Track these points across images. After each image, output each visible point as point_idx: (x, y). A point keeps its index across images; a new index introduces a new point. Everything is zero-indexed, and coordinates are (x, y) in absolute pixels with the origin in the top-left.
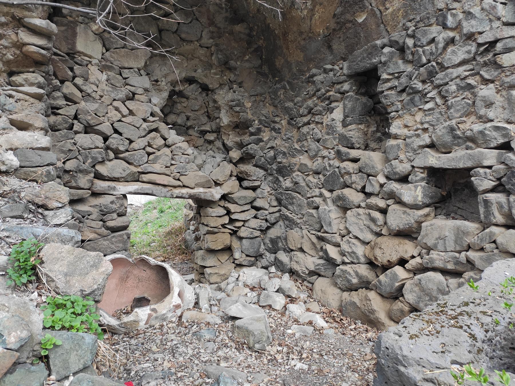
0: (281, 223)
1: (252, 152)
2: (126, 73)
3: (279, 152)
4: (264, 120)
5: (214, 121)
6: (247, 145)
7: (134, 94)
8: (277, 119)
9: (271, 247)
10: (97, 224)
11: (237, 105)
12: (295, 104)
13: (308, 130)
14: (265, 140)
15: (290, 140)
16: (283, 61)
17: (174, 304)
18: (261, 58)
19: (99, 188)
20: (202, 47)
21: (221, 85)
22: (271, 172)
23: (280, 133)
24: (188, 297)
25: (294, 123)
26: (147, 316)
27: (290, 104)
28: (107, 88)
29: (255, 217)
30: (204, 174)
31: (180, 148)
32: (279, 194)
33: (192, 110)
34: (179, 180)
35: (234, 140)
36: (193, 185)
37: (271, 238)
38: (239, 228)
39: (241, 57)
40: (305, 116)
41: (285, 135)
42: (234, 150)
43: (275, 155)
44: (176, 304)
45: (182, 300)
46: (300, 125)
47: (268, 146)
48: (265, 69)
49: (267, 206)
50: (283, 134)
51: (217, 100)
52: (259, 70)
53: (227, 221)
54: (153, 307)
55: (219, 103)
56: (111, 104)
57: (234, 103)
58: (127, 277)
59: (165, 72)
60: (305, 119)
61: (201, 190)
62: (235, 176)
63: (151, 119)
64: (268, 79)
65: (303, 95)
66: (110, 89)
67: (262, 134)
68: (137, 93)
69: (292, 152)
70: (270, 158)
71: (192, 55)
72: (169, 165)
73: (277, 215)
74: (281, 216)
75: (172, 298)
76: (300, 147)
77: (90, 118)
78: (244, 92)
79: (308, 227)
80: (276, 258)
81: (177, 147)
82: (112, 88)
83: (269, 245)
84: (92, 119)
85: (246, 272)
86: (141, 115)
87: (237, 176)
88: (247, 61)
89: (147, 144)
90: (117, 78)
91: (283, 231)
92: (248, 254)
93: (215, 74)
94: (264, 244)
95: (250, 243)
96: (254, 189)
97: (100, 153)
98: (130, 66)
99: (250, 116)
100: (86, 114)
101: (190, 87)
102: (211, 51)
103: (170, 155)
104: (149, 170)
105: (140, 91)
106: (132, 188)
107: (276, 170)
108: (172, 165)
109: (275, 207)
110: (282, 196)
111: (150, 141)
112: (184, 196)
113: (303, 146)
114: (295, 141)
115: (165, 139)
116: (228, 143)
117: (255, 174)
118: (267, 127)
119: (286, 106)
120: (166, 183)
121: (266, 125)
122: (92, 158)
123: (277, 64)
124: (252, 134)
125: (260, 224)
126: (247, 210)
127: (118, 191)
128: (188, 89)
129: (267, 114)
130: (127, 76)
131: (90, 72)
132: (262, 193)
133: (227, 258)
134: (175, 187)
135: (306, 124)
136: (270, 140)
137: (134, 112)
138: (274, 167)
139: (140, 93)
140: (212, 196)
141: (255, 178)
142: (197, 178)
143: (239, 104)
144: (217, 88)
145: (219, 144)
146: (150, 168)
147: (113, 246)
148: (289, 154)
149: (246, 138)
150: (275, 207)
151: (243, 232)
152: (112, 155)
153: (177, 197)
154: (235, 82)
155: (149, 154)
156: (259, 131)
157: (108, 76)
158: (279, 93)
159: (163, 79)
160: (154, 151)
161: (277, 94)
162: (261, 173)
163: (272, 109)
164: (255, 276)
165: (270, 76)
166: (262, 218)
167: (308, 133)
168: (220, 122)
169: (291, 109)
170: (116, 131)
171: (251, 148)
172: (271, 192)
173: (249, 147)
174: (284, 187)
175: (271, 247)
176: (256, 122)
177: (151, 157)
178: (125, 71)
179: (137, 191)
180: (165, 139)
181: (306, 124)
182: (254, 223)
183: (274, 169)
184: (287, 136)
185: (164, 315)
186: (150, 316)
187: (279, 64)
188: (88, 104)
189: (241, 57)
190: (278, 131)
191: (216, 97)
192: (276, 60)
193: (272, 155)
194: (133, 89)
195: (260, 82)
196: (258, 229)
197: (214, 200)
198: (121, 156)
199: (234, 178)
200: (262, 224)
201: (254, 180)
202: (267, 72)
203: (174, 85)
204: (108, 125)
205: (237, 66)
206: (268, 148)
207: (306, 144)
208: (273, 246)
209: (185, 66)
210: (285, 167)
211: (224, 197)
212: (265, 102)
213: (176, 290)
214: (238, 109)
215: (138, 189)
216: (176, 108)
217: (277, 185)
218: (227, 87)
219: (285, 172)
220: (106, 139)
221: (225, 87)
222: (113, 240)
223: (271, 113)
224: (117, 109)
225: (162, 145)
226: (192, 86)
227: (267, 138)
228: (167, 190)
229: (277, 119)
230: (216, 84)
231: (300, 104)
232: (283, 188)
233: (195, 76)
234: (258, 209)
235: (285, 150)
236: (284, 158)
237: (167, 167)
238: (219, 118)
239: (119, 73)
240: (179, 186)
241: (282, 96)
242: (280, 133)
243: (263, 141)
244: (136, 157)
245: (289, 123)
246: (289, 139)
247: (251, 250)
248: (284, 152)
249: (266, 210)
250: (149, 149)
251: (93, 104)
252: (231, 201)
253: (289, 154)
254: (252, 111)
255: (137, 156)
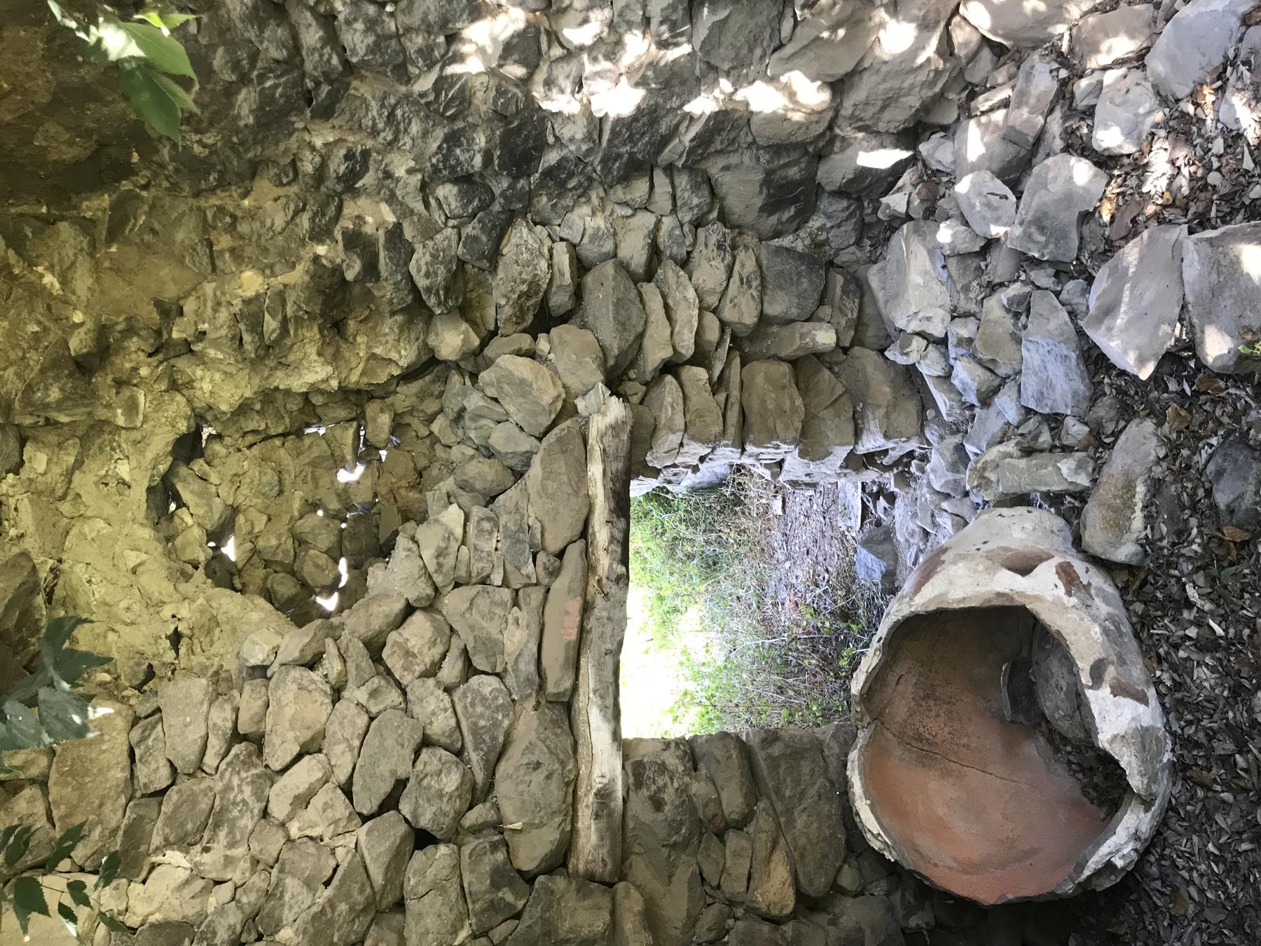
0: (714, 167)
1: (441, 271)
2: (154, 773)
3: (446, 159)
4: (312, 220)
5: (319, 411)
6: (414, 288)
7: (236, 737)
8: (308, 166)
9: (792, 211)
10: (737, 854)
11: (256, 325)
12: (244, 80)
13: (359, 26)
14: (391, 219)
15: (399, 112)
16: (52, 128)
17: (1061, 590)
18: (50, 221)
19: (604, 852)
20: (22, 463)
21: (174, 386)
22: (520, 201)
23: (366, 154)
24: (1023, 536)
25: (325, 89)
26: (1122, 700)
27: (245, 103)
28: (219, 848)
29: (685, 263)
30: (536, 460)
31: (441, 553)
32: (610, 172)
33: (281, 492)
34: (560, 555)
35: (391, 338)
36: (577, 502)
37: (762, 209)
38: (723, 325)
39: (49, 308)
40: (295, 37)
41: (374, 132)
42: (432, 341)
43: (455, 181)
44: (1060, 584)
45: (1041, 560)
46: (335, 60)
47: (419, 206)
48: (97, 205)
49: (647, 220)
50: (369, 144)
51: (236, 400)
52: (102, 232)
53: (702, 373)
54: (1085, 679)
55: (248, 394)
56: (283, 825)
57: (247, 338)
58: (919, 738)
59: (136, 607)
60: (312, 36)
61: (595, 470)
62: (535, 338)
63: (332, 665)
64: (138, 197)
65: (204, 41)
66: (222, 834)
67: (369, 229)
68: (230, 725)
69: (447, 107)
70: (465, 197)
71: (63, 498)
72: (506, 594)
73: (683, 181)
74: (689, 168)
75: (1038, 598)
76: (430, 68)
77: (343, 907)
78: (202, 299)
79: (758, 52)
80: (840, 193)
81: (440, 565)
82: (217, 826)
83: (786, 215)
84: (347, 897)
85: (913, 309)
86: (316, 709)
87: (533, 332)
88: (64, 281)
89: (431, 682)
90: (177, 808)
91: (747, 158)
92: (816, 296)
93: (132, 408)
94: (778, 234)
95: (781, 288)
96: (581, 266)
97: (476, 856)
98: (125, 759)
99: (298, 276)
100: (330, 923)
101: (190, 504)
102: (34, 426)
103: (468, 592)
104: (528, 667)
105: (221, 717)
106: (598, 729)
107: (516, 178)
108: (505, 583)
109: (652, 187)
110: (619, 156)
111: (418, 669)
112: (619, 535)
113: (426, 52)
114: (403, 89)
115: (409, 610)
116: (404, 363)
117: (528, 264)
118: (340, 208)
119: (251, 120)
120: (575, 605)
121: (331, 211)
122: (495, 886)
123: (69, 154)
124: (371, 269)
125: (712, 250)
126: (664, 297)
127: (613, 780)
128: (201, 512)
129: (286, 207)
130: (165, 772)
131: (157, 917)
132: (596, 237)
133: (827, 373)
134: (589, 568)
135: (332, 37)
136: (391, 199)
137: (307, 735)
138: (501, 185)
139: (229, 715)
140: (615, 428)
141: (544, 264)
142: (552, 487)
143: (252, 314)
144: (189, 401)
145: (405, 396)
146: (522, 666)
147: (812, 792)
148: (453, 119)
149: (386, 291)
150: (652, 187)
151: (743, 312)
152: (478, 814)
153: (625, 561)
154: (159, 333)
155: (470, 670)
156: (356, 241)
157: (168, 844)
158: (197, 149)
159: (167, 612)
160: (455, 652)
161: (202, 161)
162: (521, 237)
163: (264, 186)
164: (926, 273)
165: (126, 185)
166: (689, 240)
167: (371, 25)
168: (322, 392)
169: (266, 98)
170: (390, 803)
171: (427, 275)
172: (595, 200)
173: (422, 283)
174: (584, 147)
175: (792, 211)
176: (321, 250)
177: (479, 662)
178: (142, 772)
179: (610, 712)
180: (409, 610)
181: (332, 37)
182: (710, 271)
183: (512, 186)
184: (381, 126)
185: (1105, 631)
186: (1119, 690)
187: (71, 144)
188: (288, 916)
189: (49, 308)
190: (358, 163)
191: (224, 407)
192: (53, 156)
193: (455, 190)
194: (216, 745)
195: (154, 232)
196: (729, 258)
197: (630, 422)
198: (480, 777)
199: (543, 344)
200: (713, 239)
201: (550, 266)
202: (106, 200)
203: (189, 568)
204: (369, 833)
205: (90, 325)
206: (427, 205)
207: (419, 40)
208: (795, 200)
209: (106, 530)
210: (505, 141)
211: (615, 382)
212: (239, 214)
213: (1007, 583)
214: (271, 324)
215: (603, 709)
216: (275, 554)
217: (571, 175)
218: (183, 364)
219: (526, 140)
220: (422, 839)
221: (183, 372)
222: (788, 793)
223: (281, 191)
224: (303, 801)
225: (433, 621)
226: (186, 496)
227: (384, 208)
228: (599, 600)
229: (308, 166)
230: (174, 407)
231: (243, 54)
232: (589, 152)
233: (145, 484)
234: (655, 252)
235: (440, 133)
236: (471, 141)
237: (516, 603)
238: (306, 396)
239: (154, 801)
240: (586, 554)
241: (209, 139)
242: (366, 154)
243: (398, 226)
244: (482, 723)
245: (325, 113)
246: (392, 115)
247: (805, 283)
248: (447, 139)
249: (658, 223)
250: (451, 670)
251: (287, 897)
252: (630, 357)
253: (453, 119)
254: (277, 268)
255: (481, 716)
